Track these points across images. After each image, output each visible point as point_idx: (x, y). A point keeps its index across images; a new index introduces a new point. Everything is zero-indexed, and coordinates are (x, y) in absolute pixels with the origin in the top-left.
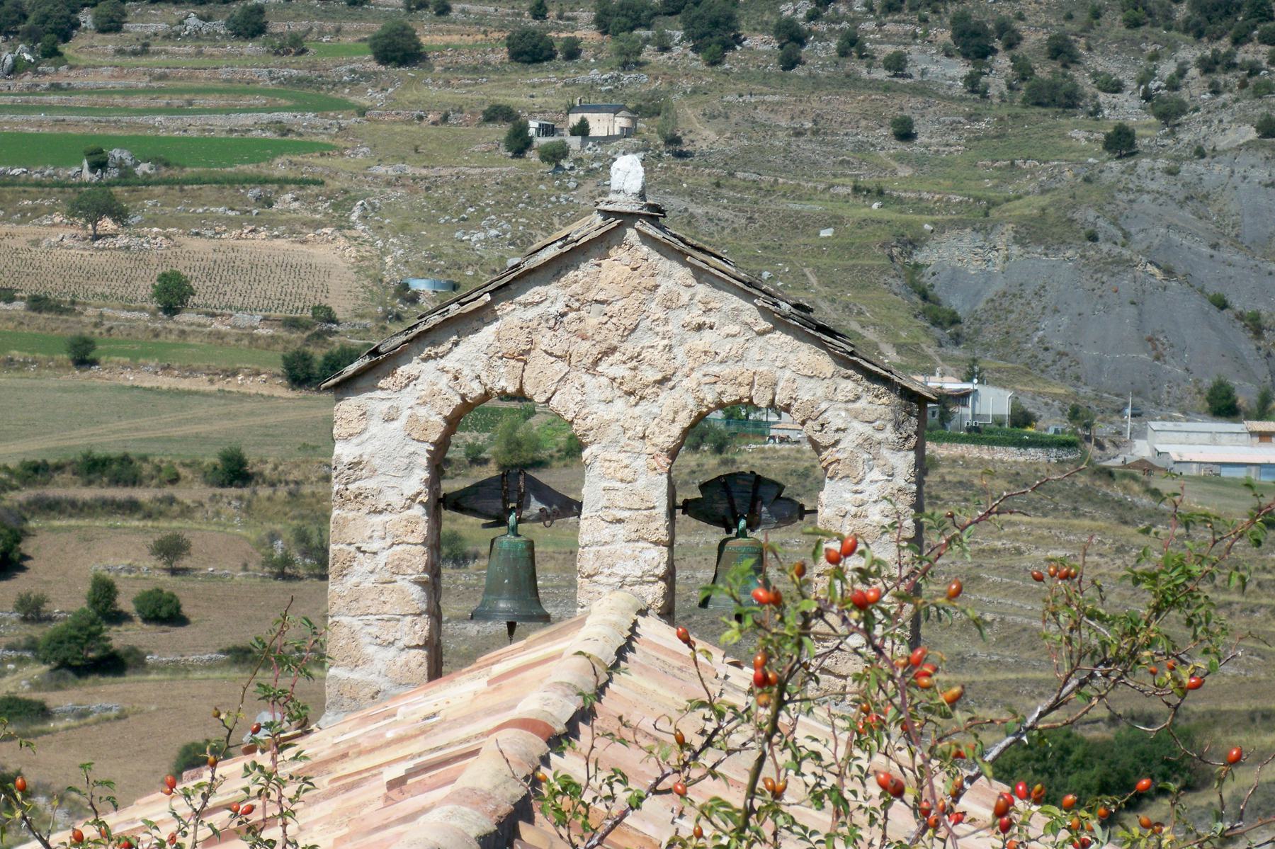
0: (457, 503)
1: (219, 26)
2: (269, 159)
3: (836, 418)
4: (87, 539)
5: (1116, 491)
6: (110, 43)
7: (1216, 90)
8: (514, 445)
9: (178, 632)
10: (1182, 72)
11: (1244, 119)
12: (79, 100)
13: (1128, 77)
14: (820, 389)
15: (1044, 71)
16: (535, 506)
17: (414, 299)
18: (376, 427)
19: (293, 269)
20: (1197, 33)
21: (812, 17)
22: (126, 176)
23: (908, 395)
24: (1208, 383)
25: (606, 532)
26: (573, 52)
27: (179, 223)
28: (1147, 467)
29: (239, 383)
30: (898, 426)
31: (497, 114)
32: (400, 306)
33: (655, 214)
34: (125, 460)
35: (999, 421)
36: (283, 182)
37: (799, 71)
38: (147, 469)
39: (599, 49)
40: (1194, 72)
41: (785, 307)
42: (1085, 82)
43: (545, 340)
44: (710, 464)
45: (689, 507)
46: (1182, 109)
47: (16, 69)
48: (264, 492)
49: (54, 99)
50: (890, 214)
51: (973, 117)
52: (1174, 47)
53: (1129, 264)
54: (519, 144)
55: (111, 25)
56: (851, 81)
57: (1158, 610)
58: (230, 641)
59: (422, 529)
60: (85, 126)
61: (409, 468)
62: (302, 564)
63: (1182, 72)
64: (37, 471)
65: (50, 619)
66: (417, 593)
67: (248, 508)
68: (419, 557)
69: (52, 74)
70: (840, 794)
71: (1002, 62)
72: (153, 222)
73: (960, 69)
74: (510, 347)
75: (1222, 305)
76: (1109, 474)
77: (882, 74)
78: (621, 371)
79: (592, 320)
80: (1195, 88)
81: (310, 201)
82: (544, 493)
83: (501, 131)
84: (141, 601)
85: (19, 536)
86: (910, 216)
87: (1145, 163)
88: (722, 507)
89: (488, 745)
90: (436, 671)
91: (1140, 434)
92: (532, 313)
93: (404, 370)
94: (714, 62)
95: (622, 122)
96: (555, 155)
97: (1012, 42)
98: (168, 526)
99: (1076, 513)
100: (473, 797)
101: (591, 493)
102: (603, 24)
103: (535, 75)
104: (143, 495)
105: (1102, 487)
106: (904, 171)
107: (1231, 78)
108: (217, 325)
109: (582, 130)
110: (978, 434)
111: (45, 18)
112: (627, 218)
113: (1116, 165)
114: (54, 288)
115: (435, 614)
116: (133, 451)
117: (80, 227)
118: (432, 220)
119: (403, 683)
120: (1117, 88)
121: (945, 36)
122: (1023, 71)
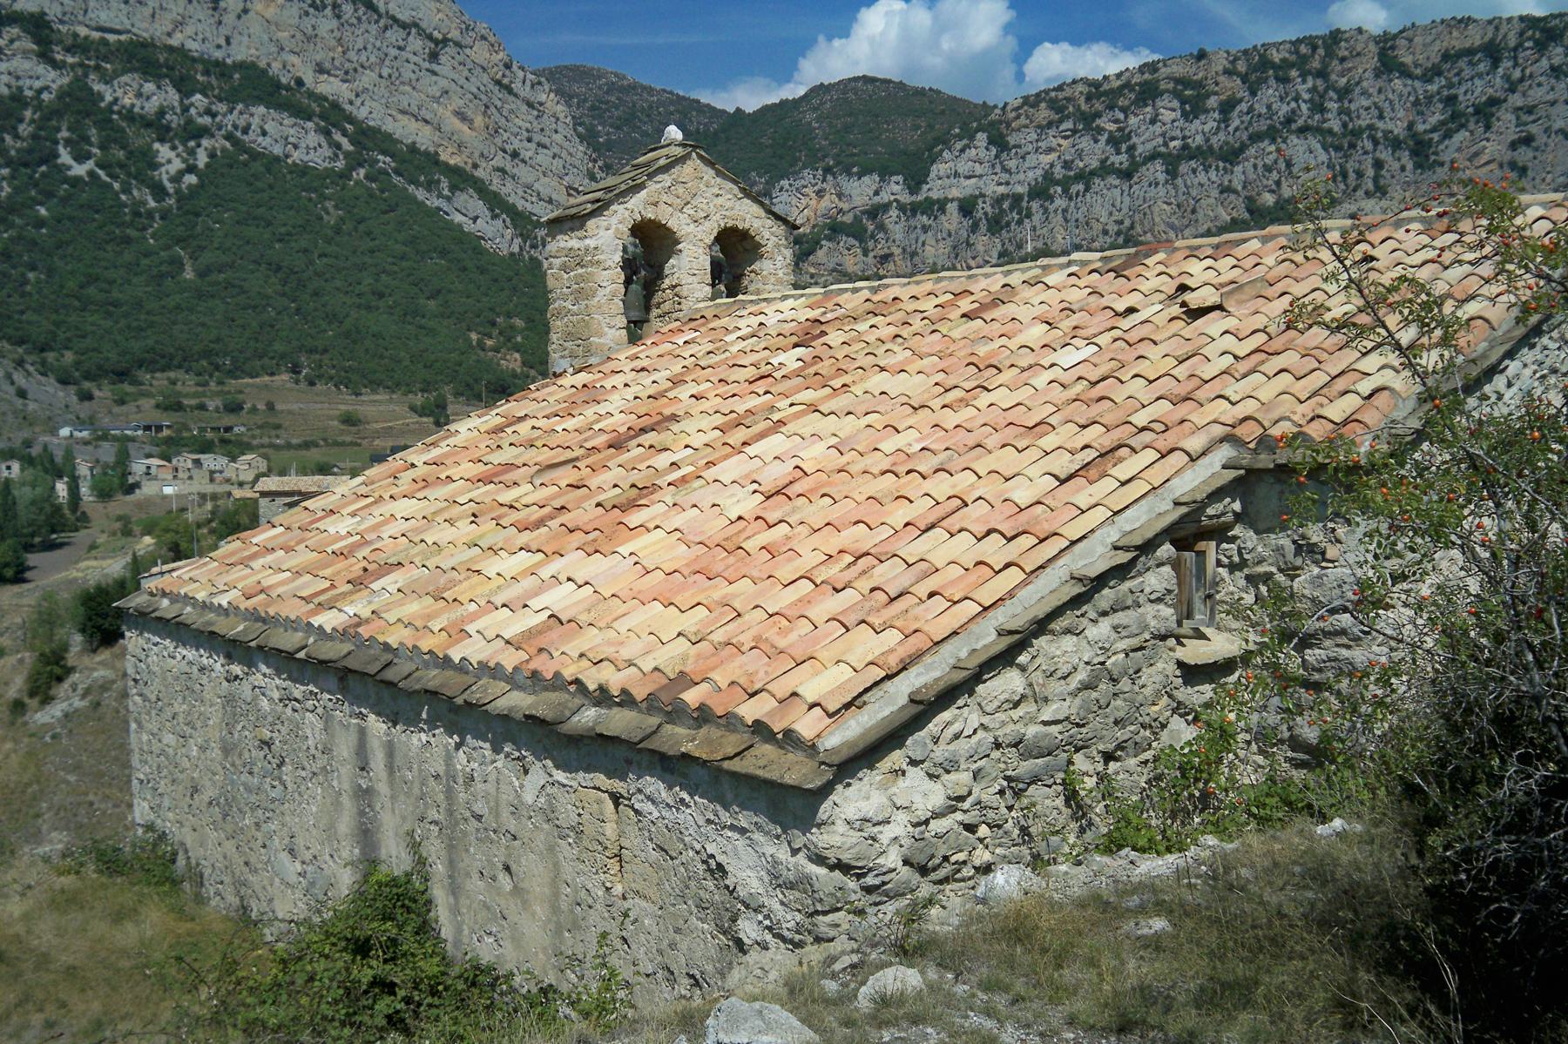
18: (602, 233)
78: (692, 212)
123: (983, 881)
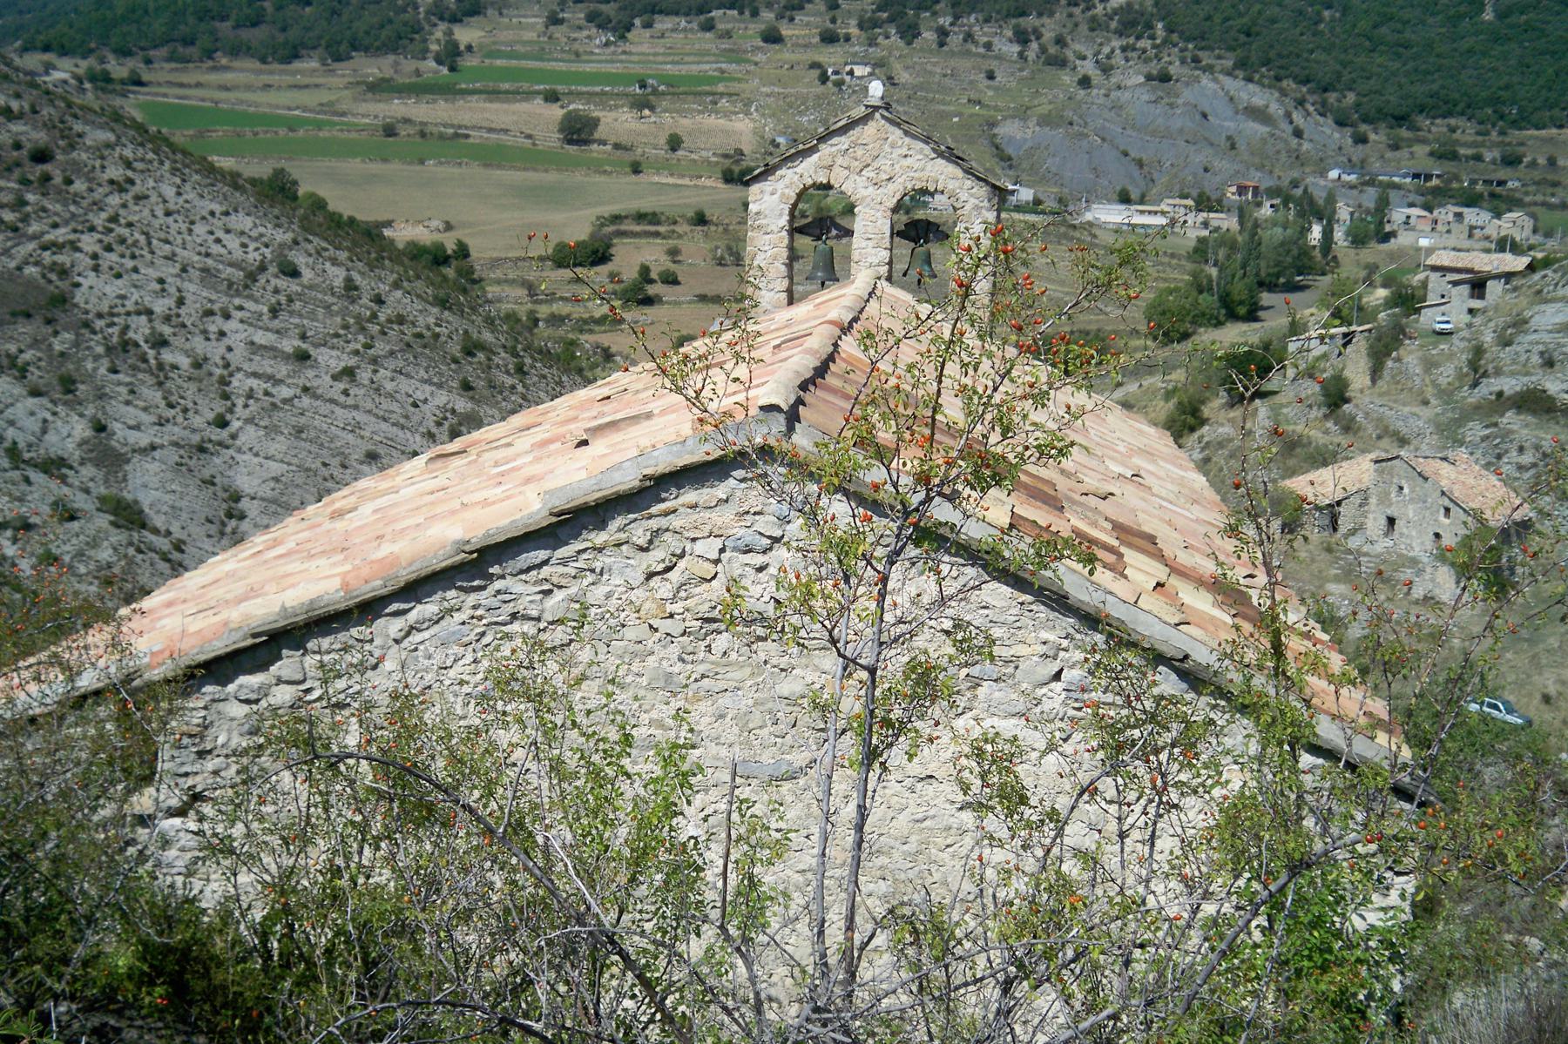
0: (801, 230)
1: (695, 25)
2: (715, 84)
3: (963, 196)
5: (1077, 234)
6: (648, 33)
7: (1127, 60)
8: (820, 209)
9: (677, 288)
10: (1113, 51)
11: (1139, 73)
13: (1089, 54)
15: (1052, 50)
16: (834, 232)
17: (778, 146)
18: (767, 197)
19: (727, 132)
20: (1120, 34)
21: (952, 24)
22: (655, 92)
23: (994, 187)
24: (1118, 188)
25: (864, 244)
26: (847, 39)
27: (677, 112)
28: (1090, 224)
29: (703, 181)
31: (815, 65)
32: (772, 149)
33: (887, 107)
34: (654, 214)
35: (1027, 203)
36: (722, 95)
37: (945, 48)
40: (1118, 51)
42: (1069, 54)
43: (839, 161)
44: (903, 218)
45: (900, 234)
46: (1112, 68)
47: (607, 44)
48: (713, 228)
50: (984, 112)
51: (1021, 70)
52: (1109, 40)
53: (1087, 136)
54: (824, 79)
55: (648, 25)
56: (968, 53)
57: (1120, 265)
58: (698, 292)
59: (786, 241)
60: (637, 69)
61: (781, 215)
62: (729, 259)
63: (1113, 51)
64: (616, 219)
65: (621, 282)
66: (783, 268)
67: (706, 235)
68: (785, 253)
69: (622, 46)
71: (1034, 45)
72: (665, 111)
73: (1016, 48)
74: (825, 163)
75: (1126, 154)
76: (1074, 227)
77: (981, 50)
78: (872, 175)
79: (860, 152)
80: (1118, 58)
82: (838, 227)
83: (816, 73)
84: (660, 275)
85: (609, 246)
86: (992, 113)
87: (1095, 91)
89: (815, 331)
90: (791, 302)
91: (1088, 209)
93: (779, 173)
94: (909, 43)
95: (868, 69)
97: (1039, 37)
98: (671, 242)
99: (1059, 243)
100: (809, 351)
101: (858, 226)
102: (861, 26)
104: (661, 229)
105: (1072, 233)
106: (990, 93)
107: (1134, 55)
108: (693, 156)
109: (851, 73)
110: (1018, 208)
111: (620, 22)
112: (876, 108)
113: (1082, 92)
114: (624, 140)
115: (791, 277)
116: (657, 210)
117: (635, 113)
119: (778, 307)
120: (1084, 58)
121: (1009, 33)
122: (1043, 50)
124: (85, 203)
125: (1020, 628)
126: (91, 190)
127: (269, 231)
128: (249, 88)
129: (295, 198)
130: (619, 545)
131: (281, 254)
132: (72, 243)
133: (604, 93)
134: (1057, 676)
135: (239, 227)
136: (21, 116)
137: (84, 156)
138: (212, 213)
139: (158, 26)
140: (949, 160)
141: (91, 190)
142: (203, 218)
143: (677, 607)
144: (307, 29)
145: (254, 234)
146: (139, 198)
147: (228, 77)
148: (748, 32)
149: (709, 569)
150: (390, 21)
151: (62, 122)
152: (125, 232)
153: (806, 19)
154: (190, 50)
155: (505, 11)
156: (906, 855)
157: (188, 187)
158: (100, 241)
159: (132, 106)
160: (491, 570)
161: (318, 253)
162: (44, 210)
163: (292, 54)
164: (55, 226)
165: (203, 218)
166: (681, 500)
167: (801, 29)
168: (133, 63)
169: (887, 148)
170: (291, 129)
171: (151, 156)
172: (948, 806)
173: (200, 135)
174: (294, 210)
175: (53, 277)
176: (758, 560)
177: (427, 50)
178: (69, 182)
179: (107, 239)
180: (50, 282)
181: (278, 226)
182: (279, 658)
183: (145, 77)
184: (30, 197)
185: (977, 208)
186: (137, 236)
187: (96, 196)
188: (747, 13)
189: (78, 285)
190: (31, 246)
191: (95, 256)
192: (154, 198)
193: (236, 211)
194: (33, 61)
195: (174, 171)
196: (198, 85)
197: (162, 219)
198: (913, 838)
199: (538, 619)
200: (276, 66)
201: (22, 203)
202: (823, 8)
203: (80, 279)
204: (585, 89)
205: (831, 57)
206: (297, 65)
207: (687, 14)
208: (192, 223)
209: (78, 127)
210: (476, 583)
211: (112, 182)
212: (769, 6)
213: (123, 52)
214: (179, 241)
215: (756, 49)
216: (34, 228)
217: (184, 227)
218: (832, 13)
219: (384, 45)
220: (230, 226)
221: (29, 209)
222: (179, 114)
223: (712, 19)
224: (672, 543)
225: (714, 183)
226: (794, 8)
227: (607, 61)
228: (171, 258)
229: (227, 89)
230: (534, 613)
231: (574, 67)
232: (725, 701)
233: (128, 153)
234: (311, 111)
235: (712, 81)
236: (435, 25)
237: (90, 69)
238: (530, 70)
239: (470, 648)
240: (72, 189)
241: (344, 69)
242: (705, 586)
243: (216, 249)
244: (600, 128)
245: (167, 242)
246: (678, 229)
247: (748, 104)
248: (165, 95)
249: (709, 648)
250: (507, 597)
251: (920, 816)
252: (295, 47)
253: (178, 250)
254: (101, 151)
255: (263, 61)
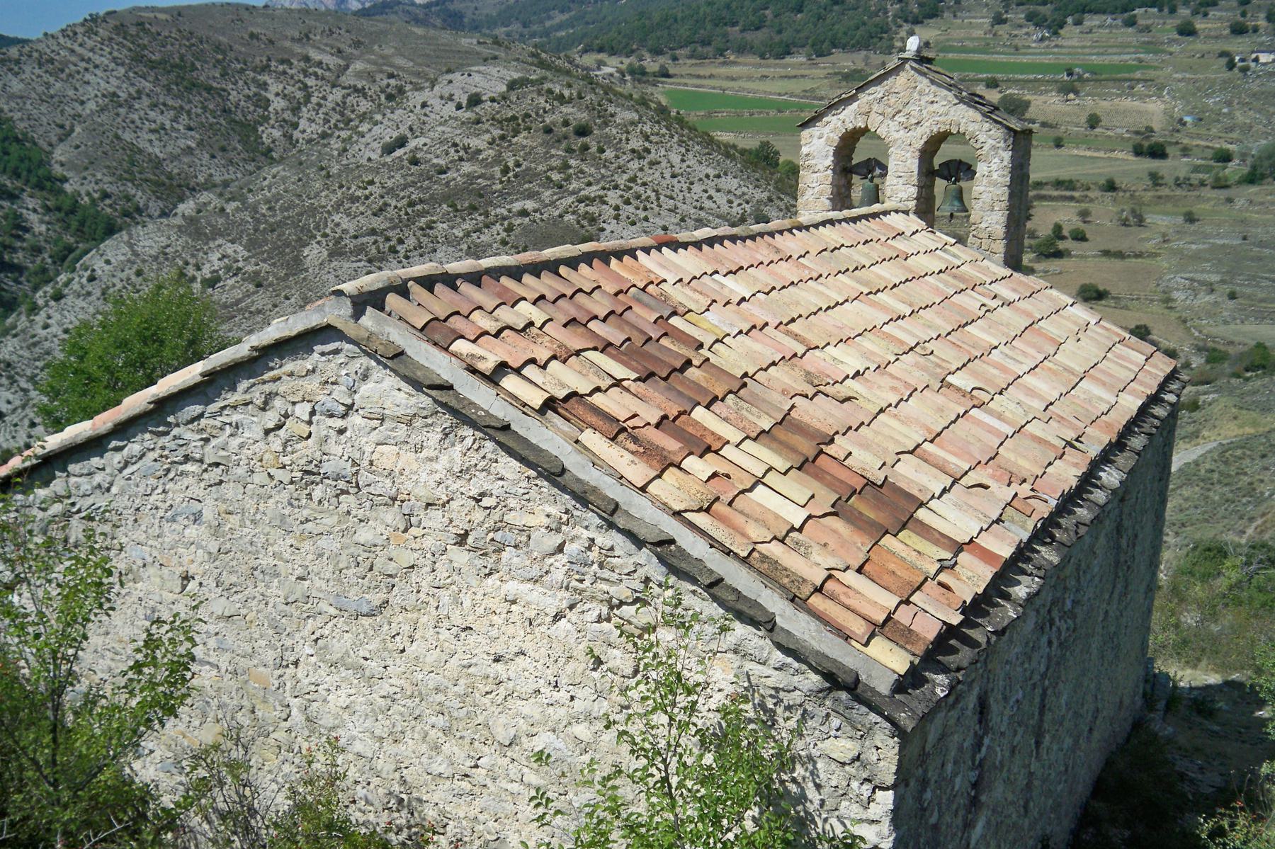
1: (1119, 22)
3: (982, 138)
4: (1054, 210)
6: (1078, 29)
9: (1084, 244)
12: (1064, 51)
14: (977, 126)
17: (1184, 124)
18: (815, 141)
19: (1139, 112)
22: (1080, 78)
25: (895, 181)
27: (1099, 95)
30: (1005, 141)
31: (1223, 54)
34: (1071, 181)
36: (1138, 81)
38: (1078, 185)
39: (1266, 28)
41: (964, 94)
43: (875, 108)
47: (1042, 39)
48: (1121, 194)
49: (1056, 50)
54: (1231, 65)
55: (1078, 23)
60: (1067, 60)
61: (827, 156)
67: (1115, 200)
70: (222, 235)
72: (1087, 95)
74: (863, 110)
78: (903, 119)
79: (893, 99)
81: (1148, 87)
83: (1224, 61)
84: (1072, 232)
88: (946, 173)
92: (871, 97)
93: (825, 119)
96: (1244, 70)
103: (1240, 39)
104: (1076, 194)
108: (1109, 133)
109: (1256, 60)
111: (1054, 21)
114: (1051, 119)
117: (1061, 97)
118: (1194, 94)
123: (1213, 467)
124: (612, 167)
125: (528, 500)
126: (617, 157)
127: (750, 190)
128: (750, 78)
129: (777, 164)
130: (246, 404)
131: (758, 210)
132: (601, 197)
133: (1036, 80)
134: (560, 549)
135: (727, 187)
136: (570, 101)
137: (614, 131)
138: (707, 176)
139: (684, 31)
140: (970, 106)
141: (617, 157)
142: (700, 180)
143: (287, 460)
144: (798, 31)
145: (738, 192)
146: (653, 164)
147: (735, 70)
148: (1163, 25)
149: (304, 430)
150: (864, 24)
151: (600, 105)
152: (640, 189)
153: (1218, 14)
154: (709, 50)
155: (959, 14)
156: (458, 695)
157: (690, 155)
158: (622, 196)
159: (660, 94)
160: (169, 419)
161: (787, 208)
162: (582, 172)
163: (786, 51)
164: (589, 184)
165: (700, 180)
166: (285, 369)
167: (1212, 24)
168: (662, 60)
169: (916, 95)
170: (780, 111)
171: (664, 131)
172: (486, 657)
173: (709, 115)
174: (772, 174)
175: (585, 223)
176: (339, 423)
177: (892, 47)
178: (602, 151)
179: (626, 195)
180: (583, 227)
181: (757, 187)
182: (54, 478)
183: (671, 71)
184: (573, 162)
185: (994, 148)
186: (649, 192)
187: (621, 161)
188: (1166, 10)
189: (603, 230)
190: (571, 199)
191: (617, 208)
192: (664, 164)
193: (726, 174)
194: (589, 60)
195: (680, 143)
196: (711, 76)
197: (669, 180)
198: (462, 682)
199: (201, 461)
200: (772, 61)
201: (566, 166)
202: (1235, 4)
203: (605, 225)
204: (1021, 77)
205: (1238, 46)
206: (788, 60)
207: (1112, 13)
208: (692, 183)
209: (611, 109)
210: (161, 429)
211: (633, 151)
212: (1186, 3)
213: (657, 52)
214: (681, 197)
215: (1172, 41)
216: (574, 185)
217: (685, 186)
218: (1242, 8)
219: (858, 42)
220: (720, 186)
221: (571, 171)
222: (696, 99)
223: (1135, 16)
224: (278, 403)
225: (1124, 156)
226: (1208, 5)
227: (1041, 54)
228: (673, 210)
229: (733, 79)
230: (198, 456)
231: (1012, 59)
232: (323, 542)
233: (647, 129)
234: (795, 96)
235: (1131, 69)
236: (900, 26)
237: (630, 64)
238: (978, 61)
239: (161, 481)
240: (603, 156)
241: (824, 62)
242: (304, 443)
243: (708, 204)
244: (1031, 109)
245: (672, 198)
246: (1091, 194)
247: (1161, 89)
248: (686, 85)
249: (309, 497)
250: (181, 442)
251: (465, 662)
252: (788, 46)
253: (679, 205)
254: (627, 127)
255: (762, 57)
